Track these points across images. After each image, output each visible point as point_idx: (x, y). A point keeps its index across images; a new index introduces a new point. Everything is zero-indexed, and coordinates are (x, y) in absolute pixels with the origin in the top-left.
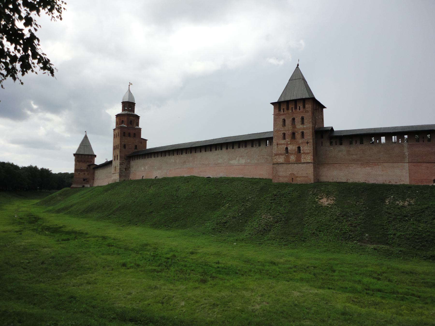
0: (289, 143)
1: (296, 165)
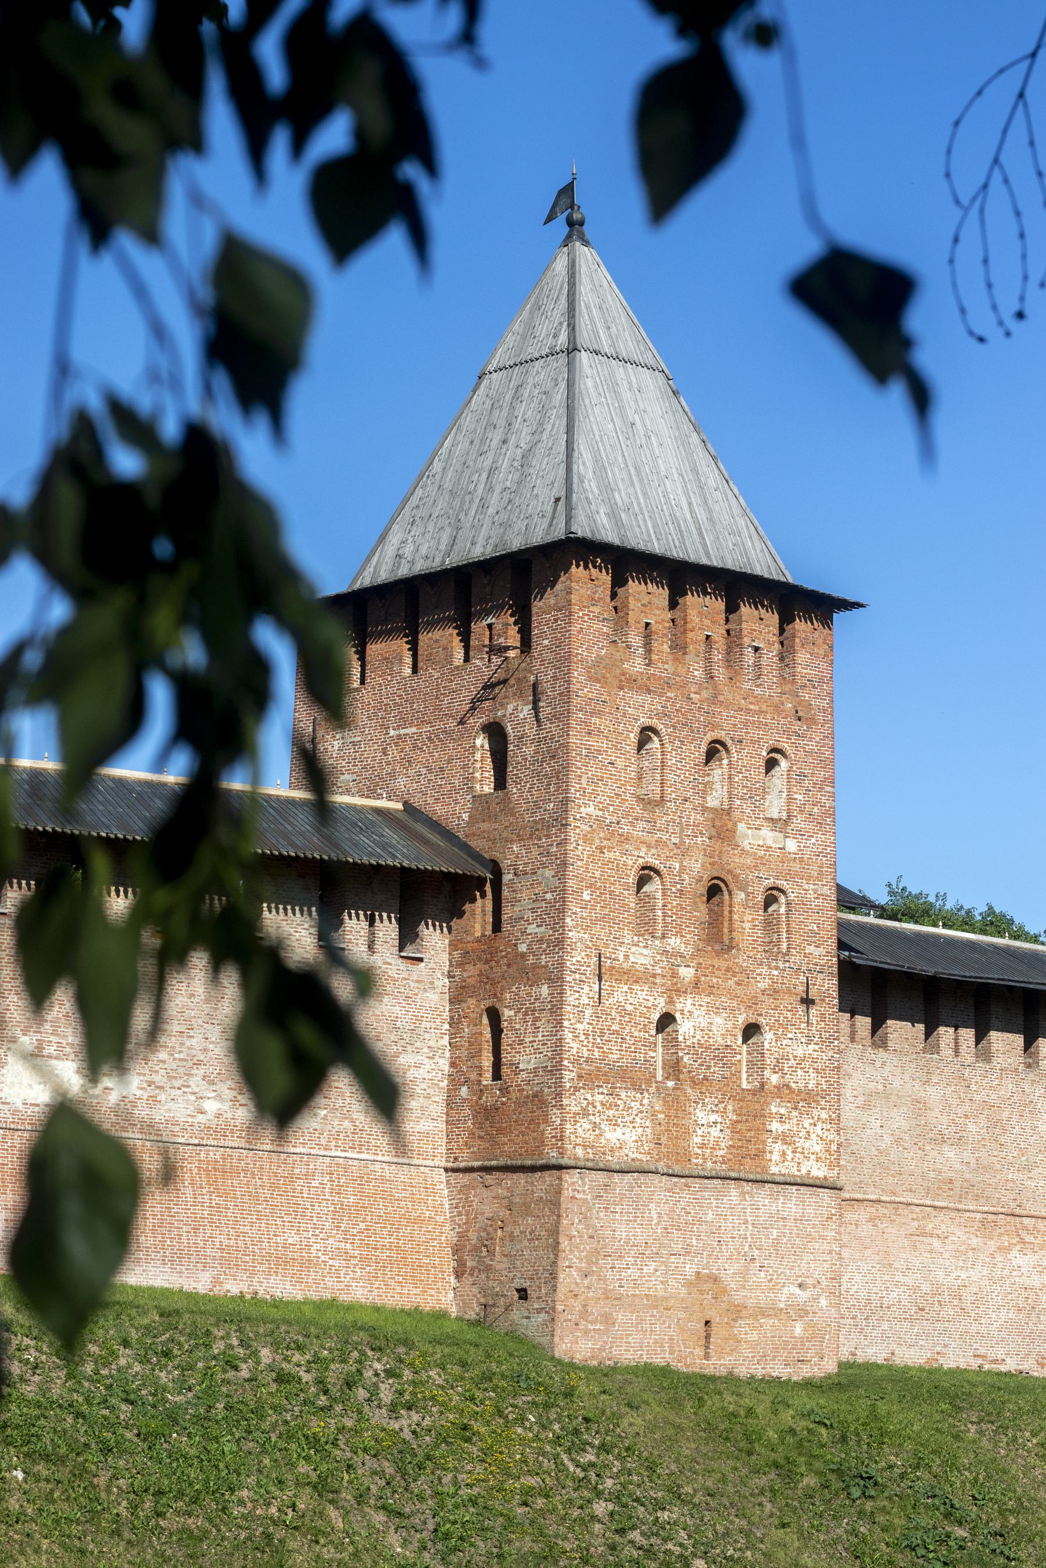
0: (687, 973)
1: (733, 1191)
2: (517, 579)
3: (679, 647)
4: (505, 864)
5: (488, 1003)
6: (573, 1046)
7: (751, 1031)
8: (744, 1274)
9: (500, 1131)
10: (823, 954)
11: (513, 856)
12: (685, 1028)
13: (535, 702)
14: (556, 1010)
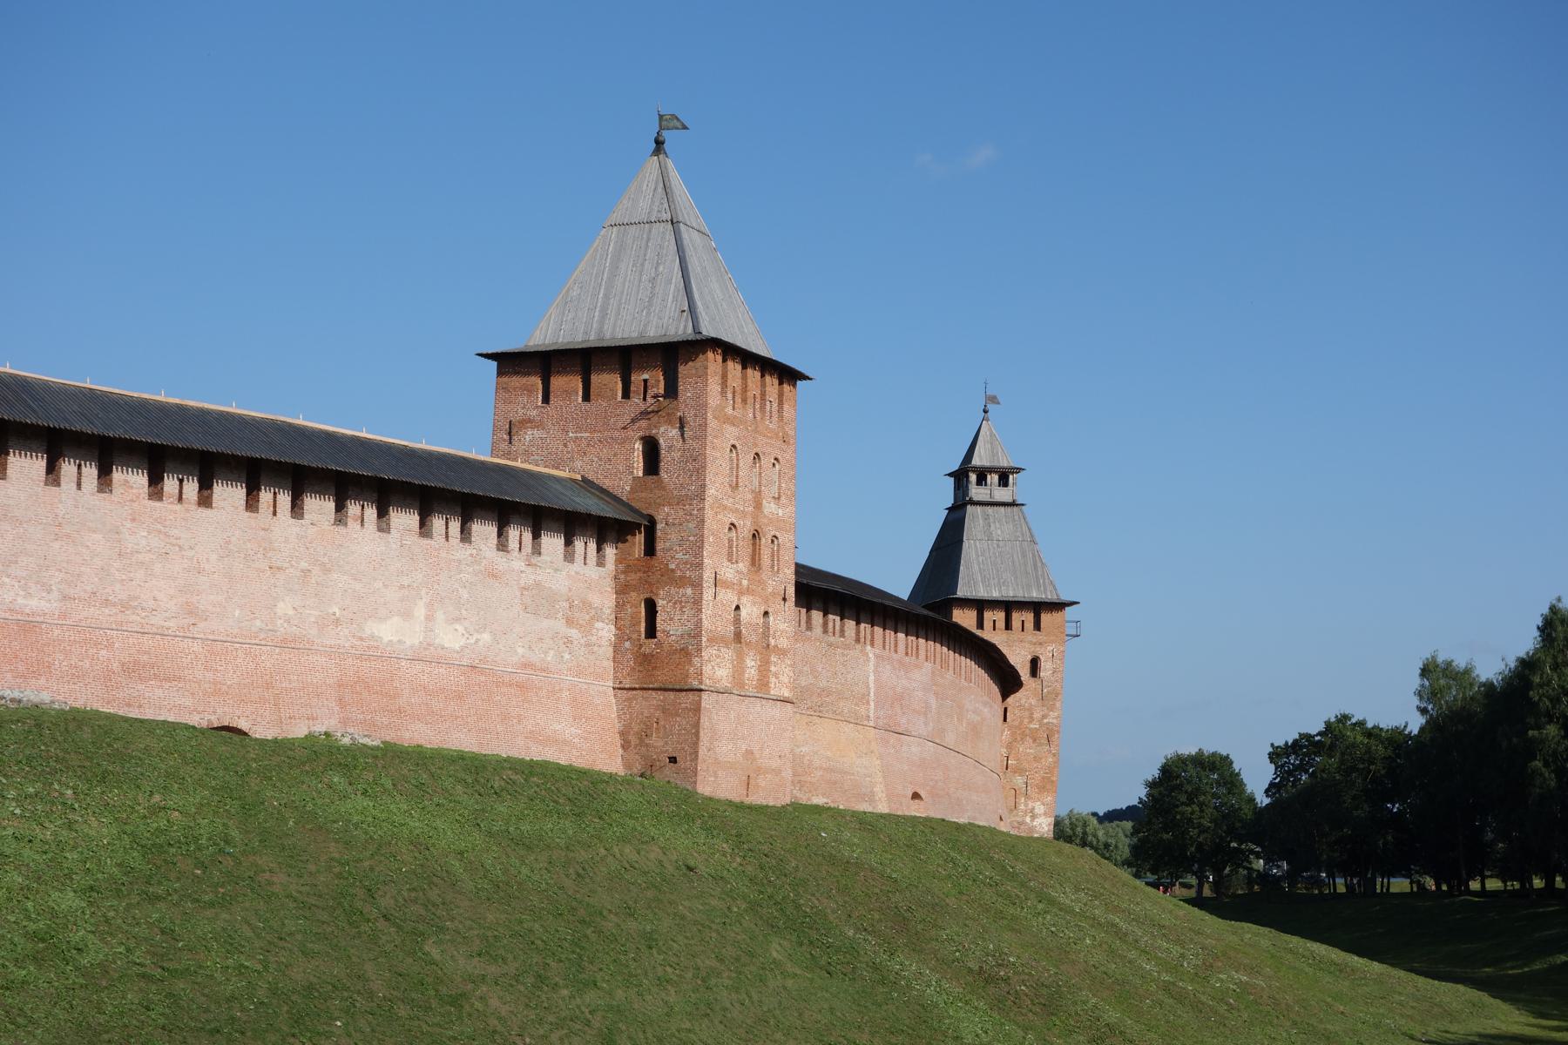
2: (671, 356)
3: (744, 401)
4: (658, 518)
5: (647, 596)
6: (706, 623)
7: (766, 613)
8: (761, 749)
9: (654, 668)
10: (789, 574)
11: (662, 514)
12: (744, 612)
13: (682, 428)
14: (697, 603)
